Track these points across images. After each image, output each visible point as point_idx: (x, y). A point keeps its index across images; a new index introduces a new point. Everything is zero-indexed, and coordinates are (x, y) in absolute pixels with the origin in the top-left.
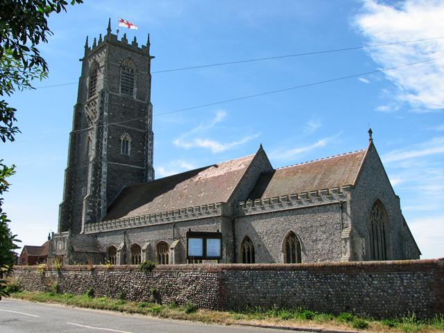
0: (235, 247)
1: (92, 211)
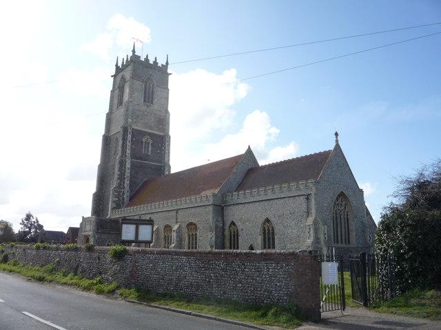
0: (224, 230)
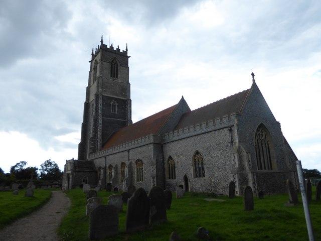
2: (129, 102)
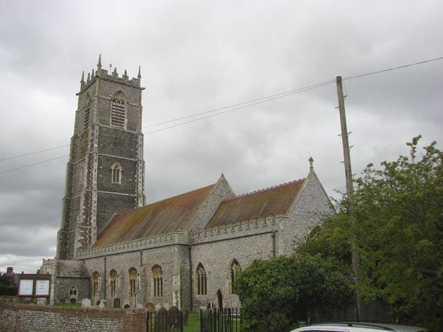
1: (83, 238)
2: (140, 165)
